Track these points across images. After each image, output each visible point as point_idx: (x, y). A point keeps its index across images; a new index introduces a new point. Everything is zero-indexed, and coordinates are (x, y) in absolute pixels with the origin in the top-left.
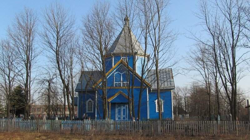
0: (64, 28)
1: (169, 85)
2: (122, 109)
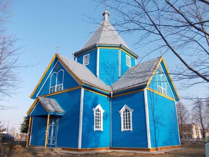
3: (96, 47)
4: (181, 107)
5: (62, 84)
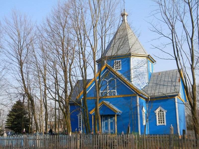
0: (77, 41)
1: (173, 91)
2: (109, 122)
3: (131, 56)
4: (16, 106)
5: (116, 91)
